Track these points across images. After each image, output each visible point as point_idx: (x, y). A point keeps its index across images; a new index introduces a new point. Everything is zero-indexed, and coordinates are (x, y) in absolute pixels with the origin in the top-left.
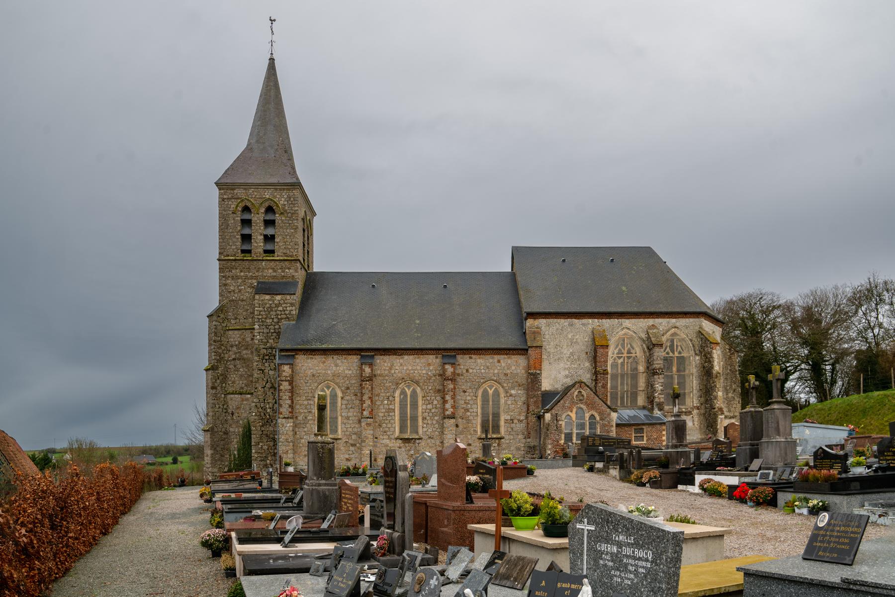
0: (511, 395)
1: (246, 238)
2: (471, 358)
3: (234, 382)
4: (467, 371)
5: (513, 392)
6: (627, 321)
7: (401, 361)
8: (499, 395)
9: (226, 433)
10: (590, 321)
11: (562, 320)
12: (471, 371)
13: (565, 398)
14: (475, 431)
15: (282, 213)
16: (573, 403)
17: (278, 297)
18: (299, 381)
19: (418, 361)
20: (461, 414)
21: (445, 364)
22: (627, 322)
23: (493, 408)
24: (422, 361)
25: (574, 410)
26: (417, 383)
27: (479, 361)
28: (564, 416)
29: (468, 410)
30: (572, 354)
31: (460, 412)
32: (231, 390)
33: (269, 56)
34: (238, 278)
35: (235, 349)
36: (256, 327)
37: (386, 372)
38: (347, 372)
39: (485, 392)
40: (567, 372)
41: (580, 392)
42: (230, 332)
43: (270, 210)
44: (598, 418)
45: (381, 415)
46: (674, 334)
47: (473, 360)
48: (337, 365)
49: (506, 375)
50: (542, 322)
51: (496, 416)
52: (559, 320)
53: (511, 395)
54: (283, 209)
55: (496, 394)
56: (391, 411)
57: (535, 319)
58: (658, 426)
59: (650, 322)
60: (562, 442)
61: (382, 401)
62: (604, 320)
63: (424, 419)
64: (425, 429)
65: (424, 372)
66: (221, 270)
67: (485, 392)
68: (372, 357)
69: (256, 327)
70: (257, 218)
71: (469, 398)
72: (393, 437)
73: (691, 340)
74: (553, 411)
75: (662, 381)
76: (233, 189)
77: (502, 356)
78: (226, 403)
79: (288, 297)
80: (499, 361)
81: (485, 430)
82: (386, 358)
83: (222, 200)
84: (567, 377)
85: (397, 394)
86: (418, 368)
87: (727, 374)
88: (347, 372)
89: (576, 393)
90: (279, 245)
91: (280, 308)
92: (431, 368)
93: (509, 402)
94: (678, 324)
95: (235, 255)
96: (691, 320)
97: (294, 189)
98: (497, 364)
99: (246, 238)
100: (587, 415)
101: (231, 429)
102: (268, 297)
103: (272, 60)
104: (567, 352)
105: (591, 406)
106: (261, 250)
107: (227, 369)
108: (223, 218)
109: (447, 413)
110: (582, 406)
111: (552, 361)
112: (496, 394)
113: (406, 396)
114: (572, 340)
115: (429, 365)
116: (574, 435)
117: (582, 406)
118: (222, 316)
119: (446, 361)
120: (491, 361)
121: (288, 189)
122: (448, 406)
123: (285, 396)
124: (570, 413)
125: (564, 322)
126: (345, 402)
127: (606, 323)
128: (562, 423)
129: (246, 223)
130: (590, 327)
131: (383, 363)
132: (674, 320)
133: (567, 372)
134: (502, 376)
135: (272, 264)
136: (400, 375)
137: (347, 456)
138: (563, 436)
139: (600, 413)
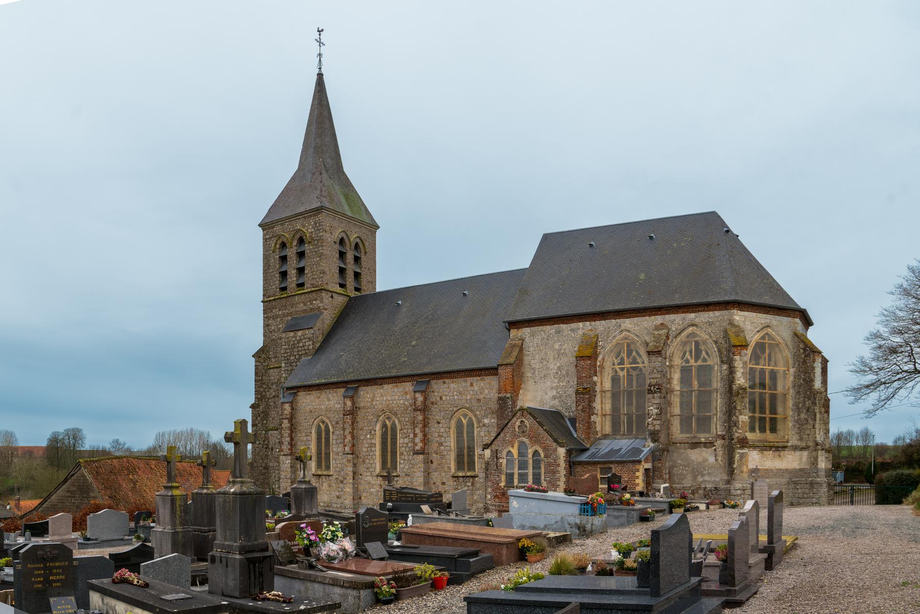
0: (484, 425)
1: (284, 275)
2: (444, 383)
3: (273, 419)
4: (441, 398)
5: (486, 421)
6: (628, 321)
7: (382, 391)
8: (473, 425)
9: (266, 468)
10: (581, 324)
11: (548, 327)
12: (444, 398)
13: (506, 430)
14: (449, 467)
15: (309, 242)
16: (515, 436)
17: (300, 333)
18: (300, 418)
19: (396, 390)
20: (435, 449)
21: (415, 392)
22: (627, 323)
23: (468, 441)
24: (400, 390)
25: (516, 445)
26: (396, 414)
27: (452, 386)
28: (505, 453)
29: (441, 444)
30: (559, 368)
31: (434, 446)
32: (271, 426)
33: (317, 71)
34: (277, 316)
35: (274, 386)
36: (283, 365)
37: (369, 404)
38: (336, 406)
39: (459, 422)
40: (554, 393)
41: (522, 421)
42: (272, 371)
43: (301, 241)
44: (542, 455)
45: (365, 450)
46: (693, 335)
47: (446, 385)
48: (329, 400)
49: (479, 400)
50: (526, 332)
51: (471, 450)
52: (544, 328)
53: (484, 425)
54: (311, 236)
55: (471, 424)
56: (372, 445)
57: (518, 328)
58: (630, 465)
59: (658, 319)
60: (502, 484)
61: (366, 436)
62: (598, 323)
63: (402, 454)
64: (402, 466)
65: (402, 402)
66: (265, 311)
67: (459, 422)
68: (356, 389)
69: (283, 365)
70: (291, 252)
71: (442, 430)
72: (375, 474)
73: (716, 342)
74: (493, 446)
75: (658, 401)
76: (273, 228)
77: (475, 378)
78: (266, 438)
79: (307, 331)
80: (472, 385)
81: (460, 464)
82: (369, 388)
83: (265, 240)
84: (554, 398)
85: (378, 427)
86: (397, 397)
87: (800, 386)
88: (336, 406)
89: (518, 423)
90: (308, 278)
91: (301, 345)
92: (408, 397)
93: (482, 434)
94: (697, 320)
95: (274, 295)
96: (717, 313)
97: (319, 213)
98: (470, 388)
99: (284, 275)
100: (530, 452)
101: (271, 464)
102: (292, 334)
103: (320, 76)
104: (553, 366)
105: (535, 439)
106: (294, 285)
107: (268, 406)
108: (266, 258)
109: (418, 448)
110: (524, 439)
111: (537, 379)
112: (471, 424)
113: (387, 429)
114: (559, 350)
115: (406, 393)
116: (516, 476)
117: (524, 439)
118: (263, 356)
119: (418, 388)
120: (464, 384)
121: (315, 215)
122: (417, 440)
123: (286, 433)
124: (511, 449)
125: (550, 329)
126: (335, 437)
127: (600, 325)
128: (503, 461)
129: (284, 259)
130: (580, 332)
131: (367, 395)
132: (692, 315)
133: (554, 393)
134: (475, 403)
135: (303, 297)
136: (380, 406)
137: (337, 494)
138: (503, 477)
139: (545, 449)
